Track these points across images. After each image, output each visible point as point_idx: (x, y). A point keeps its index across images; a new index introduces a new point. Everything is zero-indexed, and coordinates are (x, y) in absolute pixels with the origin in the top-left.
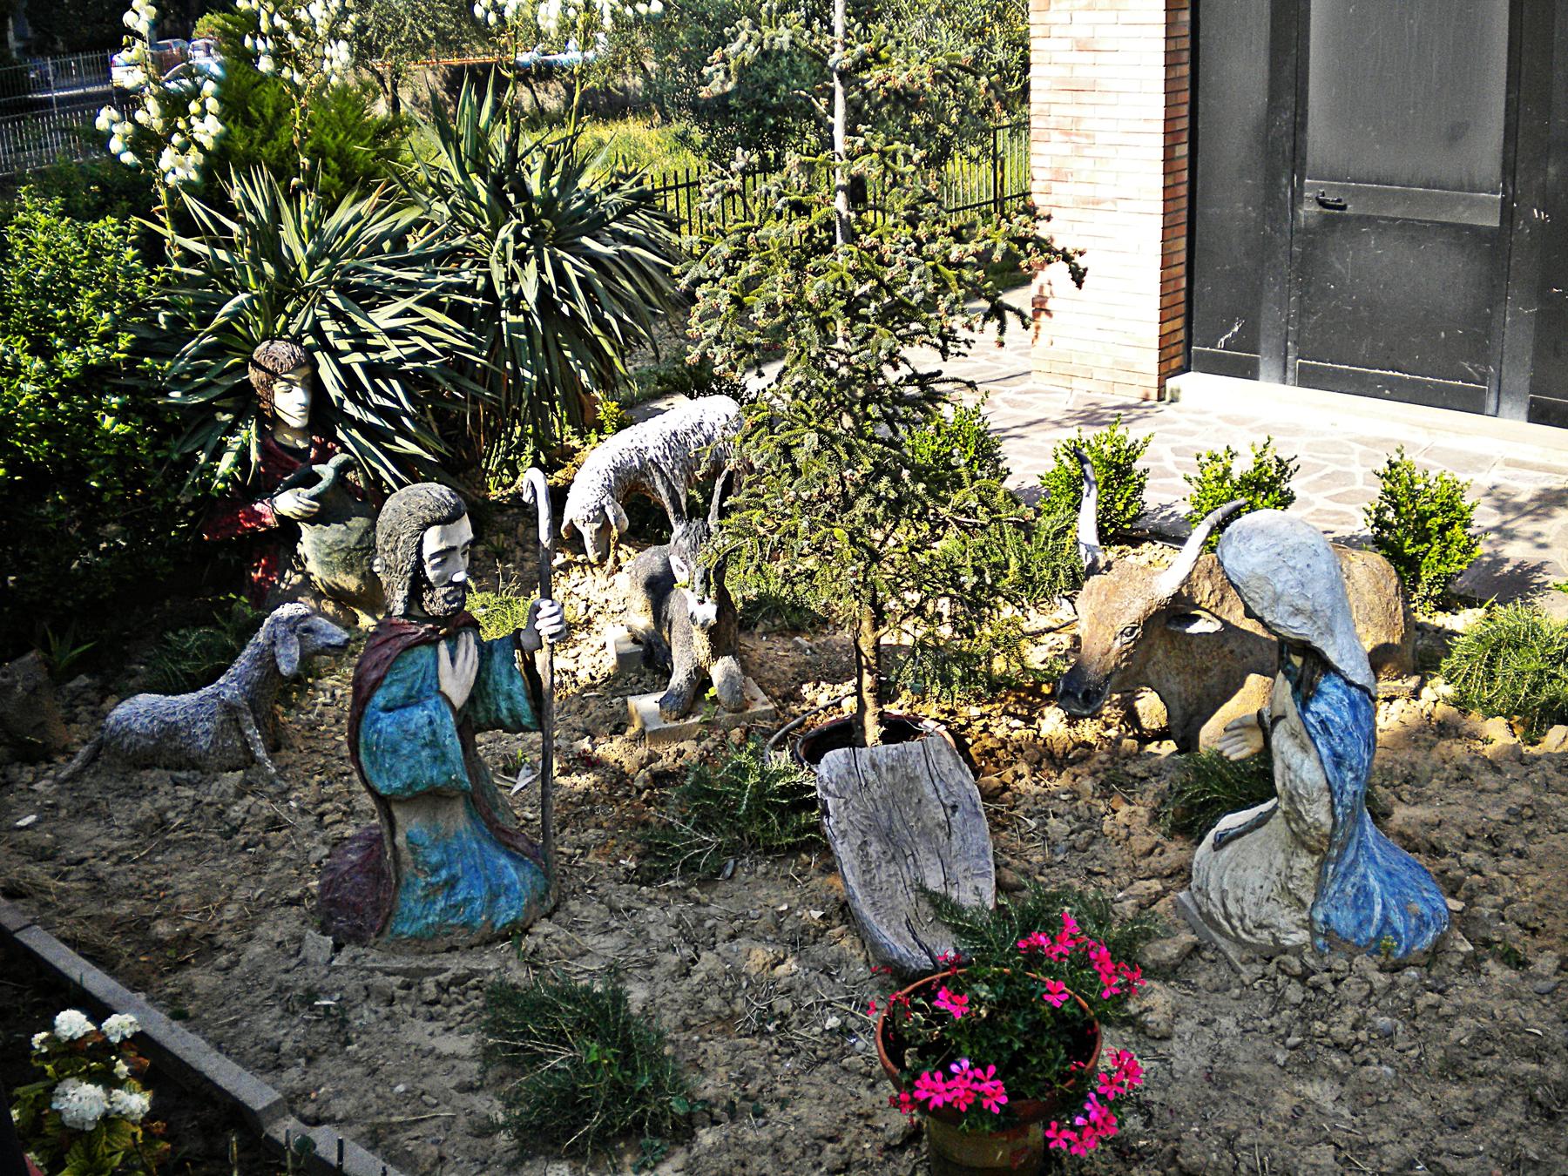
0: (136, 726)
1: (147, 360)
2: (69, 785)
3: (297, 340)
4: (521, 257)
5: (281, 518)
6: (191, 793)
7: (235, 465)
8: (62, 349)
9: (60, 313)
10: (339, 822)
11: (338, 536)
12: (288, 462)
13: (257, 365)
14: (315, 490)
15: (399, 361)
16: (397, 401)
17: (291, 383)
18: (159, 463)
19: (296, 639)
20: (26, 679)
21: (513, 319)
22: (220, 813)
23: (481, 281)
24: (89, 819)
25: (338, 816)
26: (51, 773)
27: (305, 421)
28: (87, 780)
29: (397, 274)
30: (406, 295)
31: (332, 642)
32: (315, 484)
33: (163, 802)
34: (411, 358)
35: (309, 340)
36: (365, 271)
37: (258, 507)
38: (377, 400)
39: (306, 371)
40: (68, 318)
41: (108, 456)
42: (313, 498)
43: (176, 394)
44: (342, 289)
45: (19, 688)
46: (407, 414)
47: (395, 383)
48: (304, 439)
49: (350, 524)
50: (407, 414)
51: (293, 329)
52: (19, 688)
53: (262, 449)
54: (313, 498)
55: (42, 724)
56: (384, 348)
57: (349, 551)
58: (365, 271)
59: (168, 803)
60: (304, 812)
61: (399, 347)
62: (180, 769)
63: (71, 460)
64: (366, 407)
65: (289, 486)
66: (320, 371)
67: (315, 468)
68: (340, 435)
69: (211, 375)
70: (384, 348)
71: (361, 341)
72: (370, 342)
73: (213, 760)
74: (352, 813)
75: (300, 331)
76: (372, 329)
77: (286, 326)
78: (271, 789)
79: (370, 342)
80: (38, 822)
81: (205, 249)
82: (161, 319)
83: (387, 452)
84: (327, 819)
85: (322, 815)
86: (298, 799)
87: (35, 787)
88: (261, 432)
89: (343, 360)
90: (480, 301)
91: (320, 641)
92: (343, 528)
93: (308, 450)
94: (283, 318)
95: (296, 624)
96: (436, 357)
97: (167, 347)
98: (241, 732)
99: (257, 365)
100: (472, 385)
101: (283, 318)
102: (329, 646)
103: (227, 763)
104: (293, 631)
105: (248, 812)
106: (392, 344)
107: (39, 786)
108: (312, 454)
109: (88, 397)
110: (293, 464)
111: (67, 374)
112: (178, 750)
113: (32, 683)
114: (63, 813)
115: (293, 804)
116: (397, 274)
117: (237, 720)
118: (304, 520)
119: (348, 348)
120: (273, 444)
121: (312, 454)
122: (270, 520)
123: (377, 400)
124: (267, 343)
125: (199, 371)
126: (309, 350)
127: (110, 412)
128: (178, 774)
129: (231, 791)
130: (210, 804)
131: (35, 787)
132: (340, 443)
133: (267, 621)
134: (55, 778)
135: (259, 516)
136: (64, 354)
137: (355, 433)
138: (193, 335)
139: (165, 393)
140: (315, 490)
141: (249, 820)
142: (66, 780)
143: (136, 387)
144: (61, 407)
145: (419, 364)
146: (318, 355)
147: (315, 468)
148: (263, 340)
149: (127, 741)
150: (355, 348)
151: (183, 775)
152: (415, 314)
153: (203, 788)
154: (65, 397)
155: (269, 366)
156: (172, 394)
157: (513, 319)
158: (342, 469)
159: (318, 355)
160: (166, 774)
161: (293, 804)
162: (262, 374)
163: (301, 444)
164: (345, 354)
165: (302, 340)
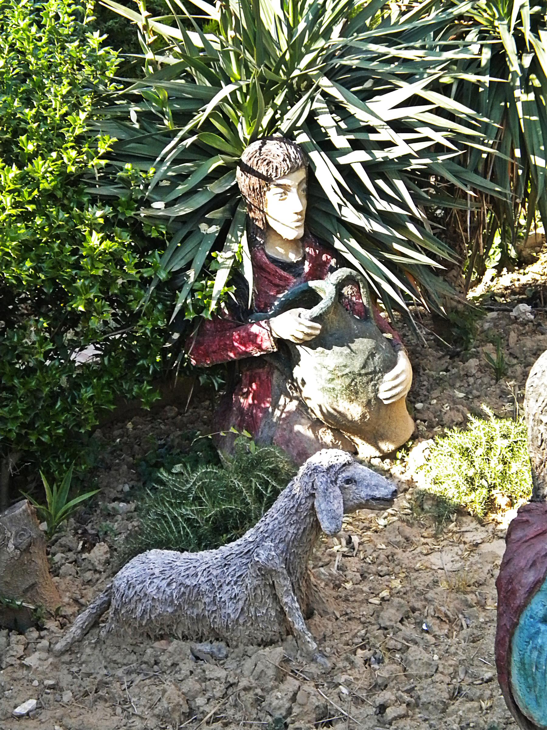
0: (151, 590)
1: (128, 166)
2: (66, 658)
3: (289, 137)
4: (306, 510)
5: (280, 342)
6: (221, 673)
7: (228, 284)
8: (35, 154)
9: (30, 113)
10: (405, 716)
11: (341, 361)
12: (281, 278)
13: (247, 170)
14: (316, 310)
15: (406, 159)
16: (403, 205)
17: (286, 188)
18: (145, 282)
19: (338, 492)
20: (18, 535)
21: (524, 97)
22: (259, 701)
23: (487, 54)
24: (100, 705)
25: (402, 709)
26: (45, 643)
27: (301, 232)
28: (88, 650)
29: (393, 52)
30: (409, 78)
31: (378, 494)
32: (316, 304)
33: (191, 685)
34: (421, 154)
35: (303, 138)
36: (359, 51)
37: (255, 329)
38: (382, 205)
39: (302, 175)
40: (39, 118)
41: (94, 276)
42: (314, 319)
43: (159, 205)
44: (331, 74)
45: (11, 546)
46: (413, 219)
47: (400, 184)
48: (297, 253)
49: (352, 346)
50: (413, 219)
51: (285, 126)
52: (11, 546)
53: (257, 267)
54: (314, 319)
55: (33, 586)
56: (390, 144)
57: (353, 376)
58: (359, 51)
59: (198, 686)
60: (358, 701)
61: (408, 142)
62: (200, 640)
63: (52, 280)
64: (363, 210)
65: (286, 307)
66: (318, 174)
67: (312, 284)
68: (338, 245)
69: (192, 181)
70: (390, 144)
71: (361, 136)
72: (373, 137)
73: (243, 632)
74: (417, 705)
75: (293, 127)
76: (373, 122)
77: (273, 122)
78: (313, 669)
79: (373, 137)
80: (39, 707)
81: (177, 33)
82: (134, 117)
83: (389, 264)
84: (391, 713)
85: (382, 708)
86: (348, 684)
87: (27, 661)
88: (251, 243)
89: (342, 160)
90: (486, 79)
91: (364, 493)
92: (345, 350)
93: (302, 263)
94: (270, 112)
95: (337, 473)
96: (450, 151)
97: (143, 150)
98: (276, 598)
99: (247, 170)
100: (478, 180)
101: (270, 112)
102: (374, 498)
103: (260, 636)
104: (334, 482)
105: (294, 699)
106: (399, 138)
107: (31, 660)
108: (307, 267)
109: (66, 209)
110: (287, 279)
111: (44, 185)
112: (200, 619)
113: (25, 541)
114: (67, 696)
115: (344, 690)
116: (393, 52)
117: (273, 586)
118: (305, 343)
119: (348, 145)
120: (265, 259)
121: (307, 267)
122: (268, 344)
123: (382, 205)
124: (258, 143)
125: (182, 177)
126: (303, 149)
127: (93, 227)
128: (199, 646)
129: (271, 673)
130: (246, 689)
131: (27, 661)
132: (336, 254)
133: (302, 470)
134: (49, 650)
135: (252, 339)
136: (39, 161)
137: (353, 243)
138: (171, 135)
139: (147, 204)
140: (316, 310)
141: (296, 710)
142: (62, 653)
143: (116, 198)
144: (38, 221)
145: (427, 161)
146: (314, 155)
147: (312, 284)
148: (254, 139)
149: (140, 608)
150: (356, 145)
151: (205, 647)
152: (423, 101)
153: (231, 664)
154: (41, 211)
155: (262, 170)
156: (155, 205)
157: (524, 97)
158: (340, 286)
159: (314, 155)
160: (186, 646)
161: (344, 690)
162: (254, 180)
163: (293, 257)
164: (343, 152)
165: (294, 138)
